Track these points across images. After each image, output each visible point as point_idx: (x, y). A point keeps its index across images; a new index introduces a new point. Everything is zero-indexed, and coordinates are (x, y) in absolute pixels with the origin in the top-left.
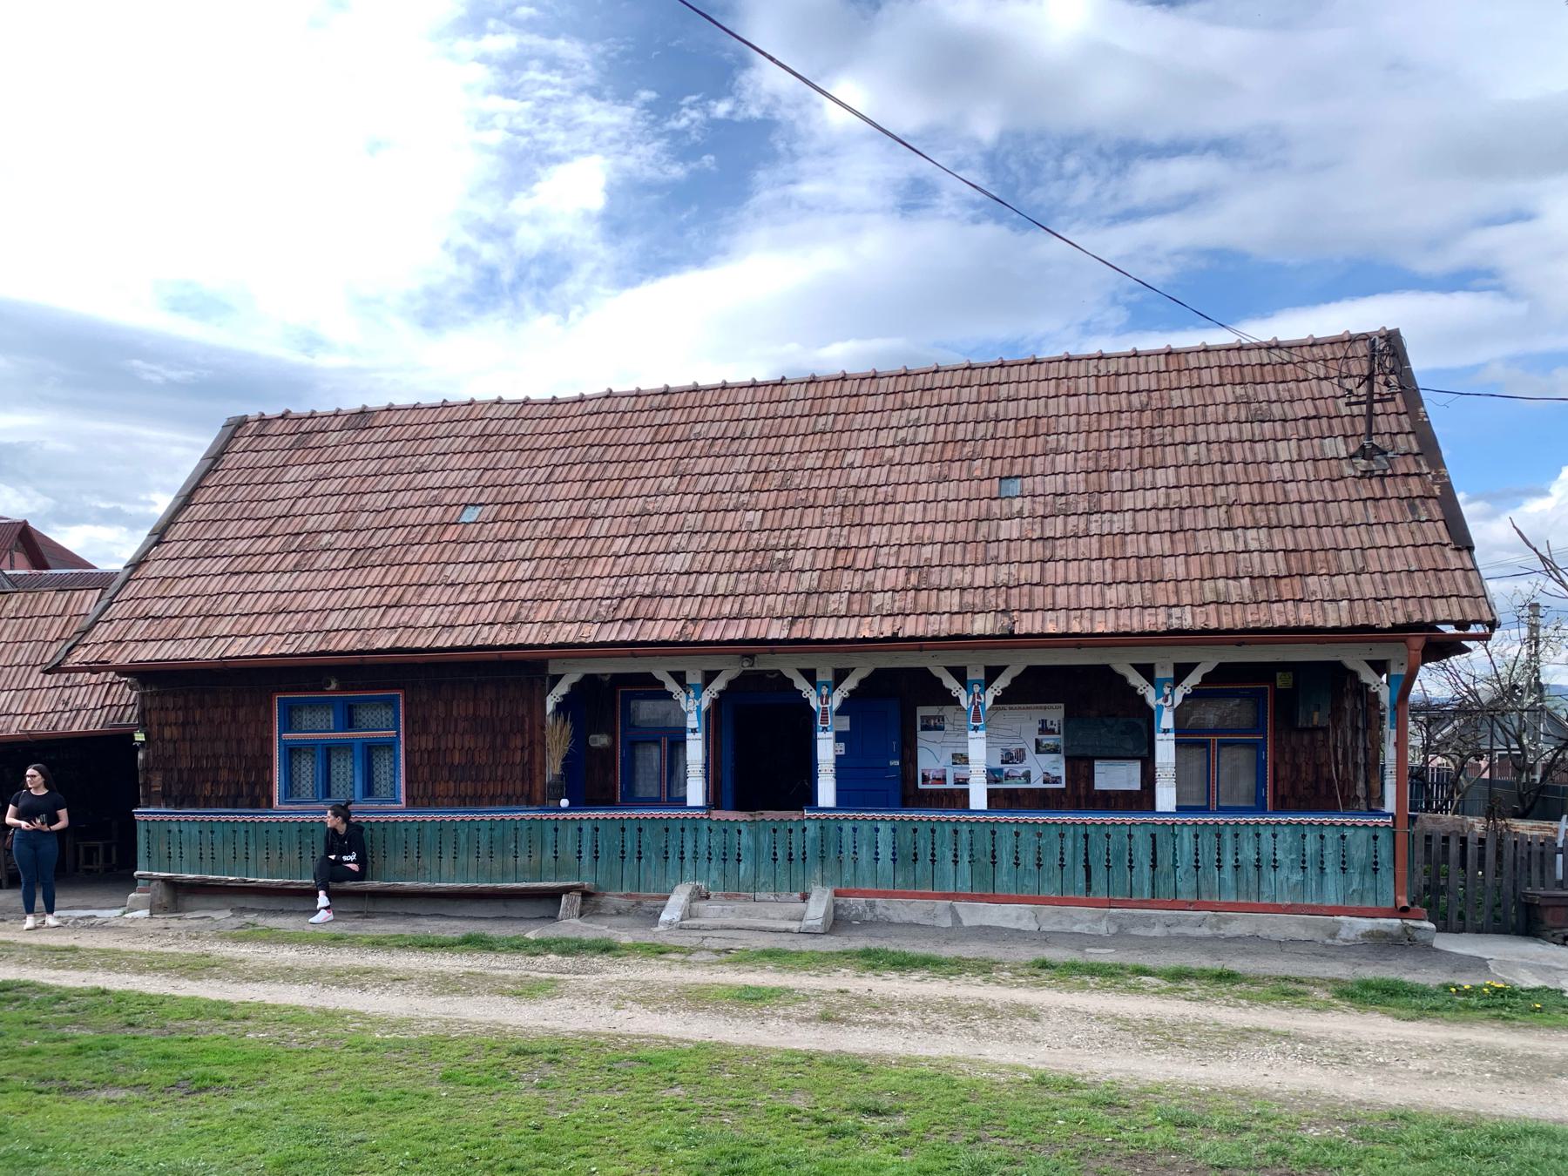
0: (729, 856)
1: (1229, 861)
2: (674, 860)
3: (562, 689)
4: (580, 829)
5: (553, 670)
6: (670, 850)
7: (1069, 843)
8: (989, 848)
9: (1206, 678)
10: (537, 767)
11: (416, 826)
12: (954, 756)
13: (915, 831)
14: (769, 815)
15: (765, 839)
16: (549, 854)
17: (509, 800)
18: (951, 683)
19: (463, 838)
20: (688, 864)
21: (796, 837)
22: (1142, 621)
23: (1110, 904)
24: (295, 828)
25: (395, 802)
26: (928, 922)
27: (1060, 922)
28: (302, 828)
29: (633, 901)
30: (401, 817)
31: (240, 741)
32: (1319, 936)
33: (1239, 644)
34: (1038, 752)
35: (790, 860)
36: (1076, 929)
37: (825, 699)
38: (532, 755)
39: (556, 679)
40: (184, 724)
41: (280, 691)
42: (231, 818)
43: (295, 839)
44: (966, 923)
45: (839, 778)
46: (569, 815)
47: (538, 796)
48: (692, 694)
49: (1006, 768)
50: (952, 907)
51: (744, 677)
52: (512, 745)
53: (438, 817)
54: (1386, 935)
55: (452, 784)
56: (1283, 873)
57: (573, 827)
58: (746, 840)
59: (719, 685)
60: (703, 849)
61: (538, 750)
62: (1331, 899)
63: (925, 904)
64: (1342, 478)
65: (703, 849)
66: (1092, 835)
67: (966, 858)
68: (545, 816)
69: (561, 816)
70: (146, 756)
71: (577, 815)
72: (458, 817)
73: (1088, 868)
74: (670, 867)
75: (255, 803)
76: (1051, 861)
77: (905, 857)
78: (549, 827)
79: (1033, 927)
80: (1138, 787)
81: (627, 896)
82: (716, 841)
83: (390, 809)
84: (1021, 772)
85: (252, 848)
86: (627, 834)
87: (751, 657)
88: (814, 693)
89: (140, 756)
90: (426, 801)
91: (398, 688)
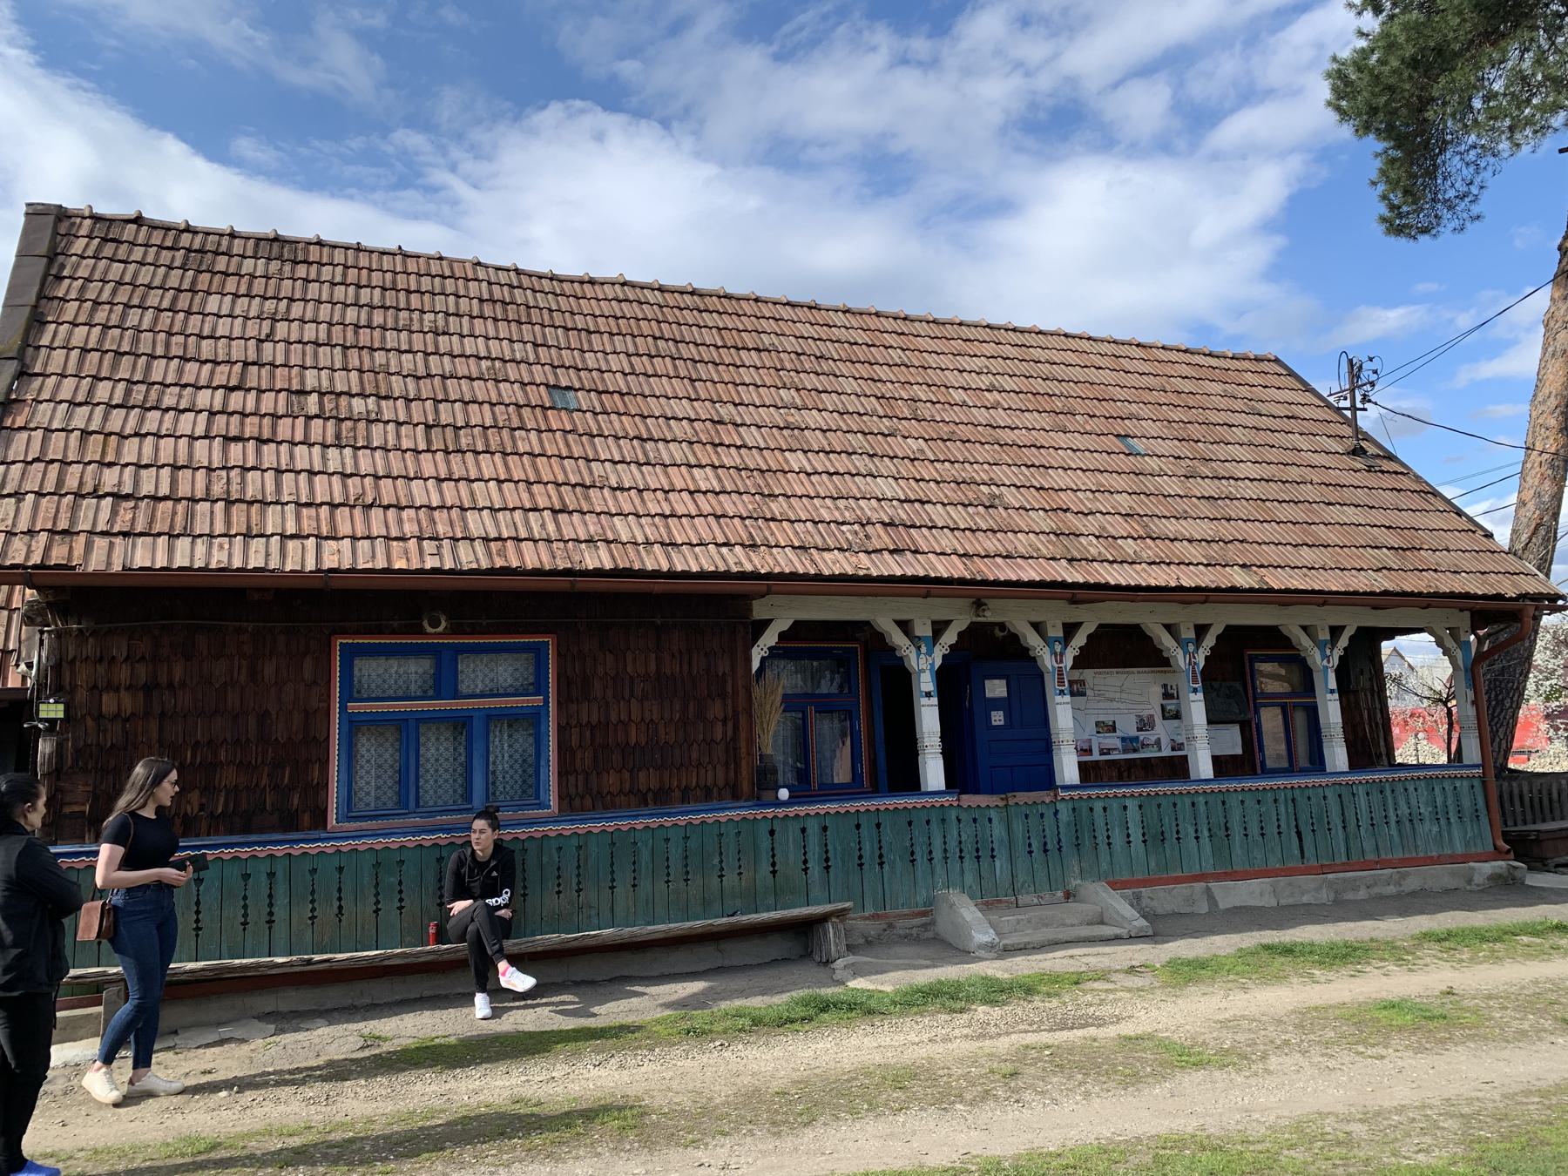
0: (982, 853)
1: (1393, 819)
2: (871, 868)
3: (769, 639)
4: (803, 830)
5: (759, 611)
6: (917, 850)
7: (1282, 809)
8: (1222, 821)
9: (783, 636)
10: (743, 744)
11: (574, 842)
12: (1097, 724)
13: (1159, 806)
14: (1022, 797)
15: (1018, 827)
16: (765, 868)
17: (707, 795)
18: (1167, 641)
19: (645, 855)
20: (939, 869)
21: (1049, 821)
22: (455, 557)
23: (1322, 870)
24: (370, 860)
25: (540, 806)
26: (1188, 910)
27: (1292, 895)
28: (380, 860)
29: (881, 924)
30: (552, 830)
31: (263, 717)
32: (1461, 883)
33: (1375, 608)
34: (1164, 718)
35: (1046, 851)
36: (1305, 899)
37: (1059, 657)
38: (736, 728)
39: (764, 625)
40: (149, 689)
41: (344, 632)
42: (245, 852)
43: (367, 879)
44: (1222, 906)
45: (947, 754)
46: (792, 811)
47: (745, 787)
48: (923, 649)
49: (1142, 735)
50: (1208, 888)
51: (973, 627)
52: (710, 716)
53: (611, 826)
54: (1500, 876)
55: (627, 775)
56: (1427, 825)
57: (793, 830)
58: (998, 830)
59: (950, 637)
60: (952, 845)
61: (742, 720)
62: (1459, 849)
63: (1182, 889)
64: (429, 376)
65: (952, 845)
66: (1299, 799)
67: (1206, 834)
68: (759, 813)
69: (781, 812)
70: (59, 750)
71: (802, 810)
72: (639, 824)
73: (1299, 834)
74: (919, 874)
75: (289, 823)
76: (1272, 829)
77: (1155, 838)
78: (763, 830)
79: (1273, 903)
80: (1239, 751)
81: (874, 917)
82: (967, 834)
83: (546, 823)
84: (1153, 739)
85: (281, 900)
86: (864, 831)
87: (979, 605)
88: (1047, 650)
89: (45, 747)
90: (588, 802)
91: (547, 632)
